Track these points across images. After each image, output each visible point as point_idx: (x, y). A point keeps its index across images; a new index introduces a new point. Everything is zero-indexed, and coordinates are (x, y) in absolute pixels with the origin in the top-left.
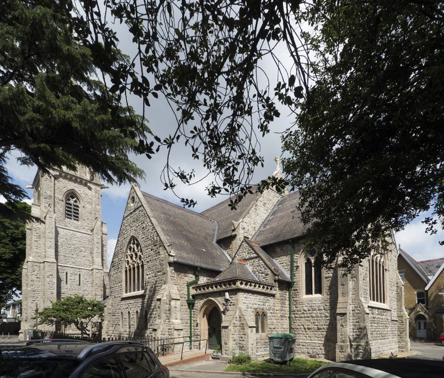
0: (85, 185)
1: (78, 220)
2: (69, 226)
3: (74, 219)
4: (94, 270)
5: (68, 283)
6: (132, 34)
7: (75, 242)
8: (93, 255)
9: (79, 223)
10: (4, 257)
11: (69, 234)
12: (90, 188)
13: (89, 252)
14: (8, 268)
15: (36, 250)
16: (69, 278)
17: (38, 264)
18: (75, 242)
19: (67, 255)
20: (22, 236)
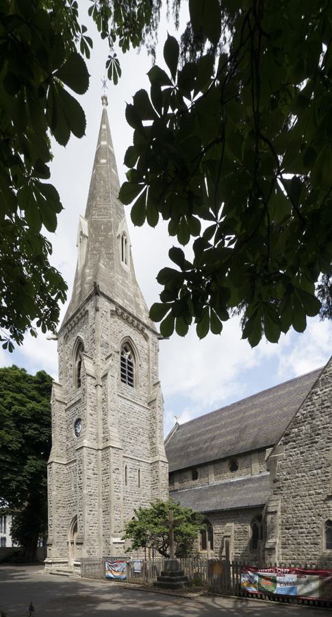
0: (142, 331)
1: (132, 386)
2: (126, 394)
3: (129, 384)
4: (160, 462)
5: (128, 484)
6: (60, 201)
7: (133, 420)
8: (154, 440)
9: (133, 391)
10: (11, 447)
11: (127, 407)
12: (146, 337)
13: (147, 436)
14: (14, 464)
15: (91, 429)
16: (128, 475)
17: (94, 452)
18: (133, 420)
19: (126, 439)
20: (31, 416)
